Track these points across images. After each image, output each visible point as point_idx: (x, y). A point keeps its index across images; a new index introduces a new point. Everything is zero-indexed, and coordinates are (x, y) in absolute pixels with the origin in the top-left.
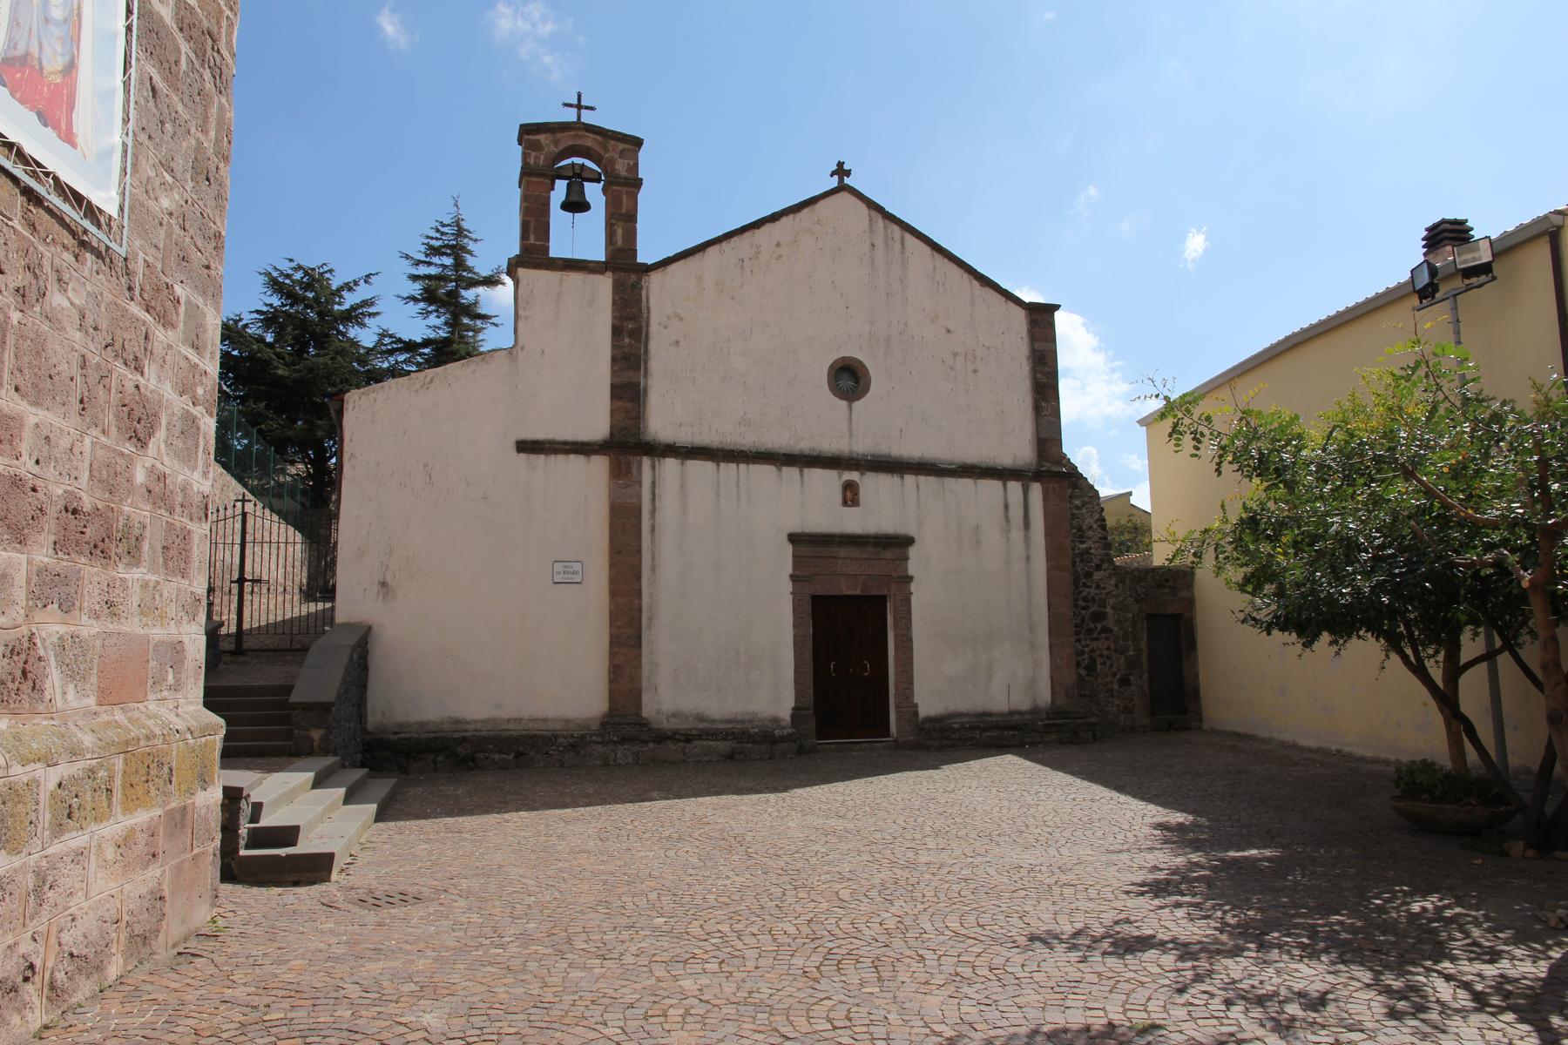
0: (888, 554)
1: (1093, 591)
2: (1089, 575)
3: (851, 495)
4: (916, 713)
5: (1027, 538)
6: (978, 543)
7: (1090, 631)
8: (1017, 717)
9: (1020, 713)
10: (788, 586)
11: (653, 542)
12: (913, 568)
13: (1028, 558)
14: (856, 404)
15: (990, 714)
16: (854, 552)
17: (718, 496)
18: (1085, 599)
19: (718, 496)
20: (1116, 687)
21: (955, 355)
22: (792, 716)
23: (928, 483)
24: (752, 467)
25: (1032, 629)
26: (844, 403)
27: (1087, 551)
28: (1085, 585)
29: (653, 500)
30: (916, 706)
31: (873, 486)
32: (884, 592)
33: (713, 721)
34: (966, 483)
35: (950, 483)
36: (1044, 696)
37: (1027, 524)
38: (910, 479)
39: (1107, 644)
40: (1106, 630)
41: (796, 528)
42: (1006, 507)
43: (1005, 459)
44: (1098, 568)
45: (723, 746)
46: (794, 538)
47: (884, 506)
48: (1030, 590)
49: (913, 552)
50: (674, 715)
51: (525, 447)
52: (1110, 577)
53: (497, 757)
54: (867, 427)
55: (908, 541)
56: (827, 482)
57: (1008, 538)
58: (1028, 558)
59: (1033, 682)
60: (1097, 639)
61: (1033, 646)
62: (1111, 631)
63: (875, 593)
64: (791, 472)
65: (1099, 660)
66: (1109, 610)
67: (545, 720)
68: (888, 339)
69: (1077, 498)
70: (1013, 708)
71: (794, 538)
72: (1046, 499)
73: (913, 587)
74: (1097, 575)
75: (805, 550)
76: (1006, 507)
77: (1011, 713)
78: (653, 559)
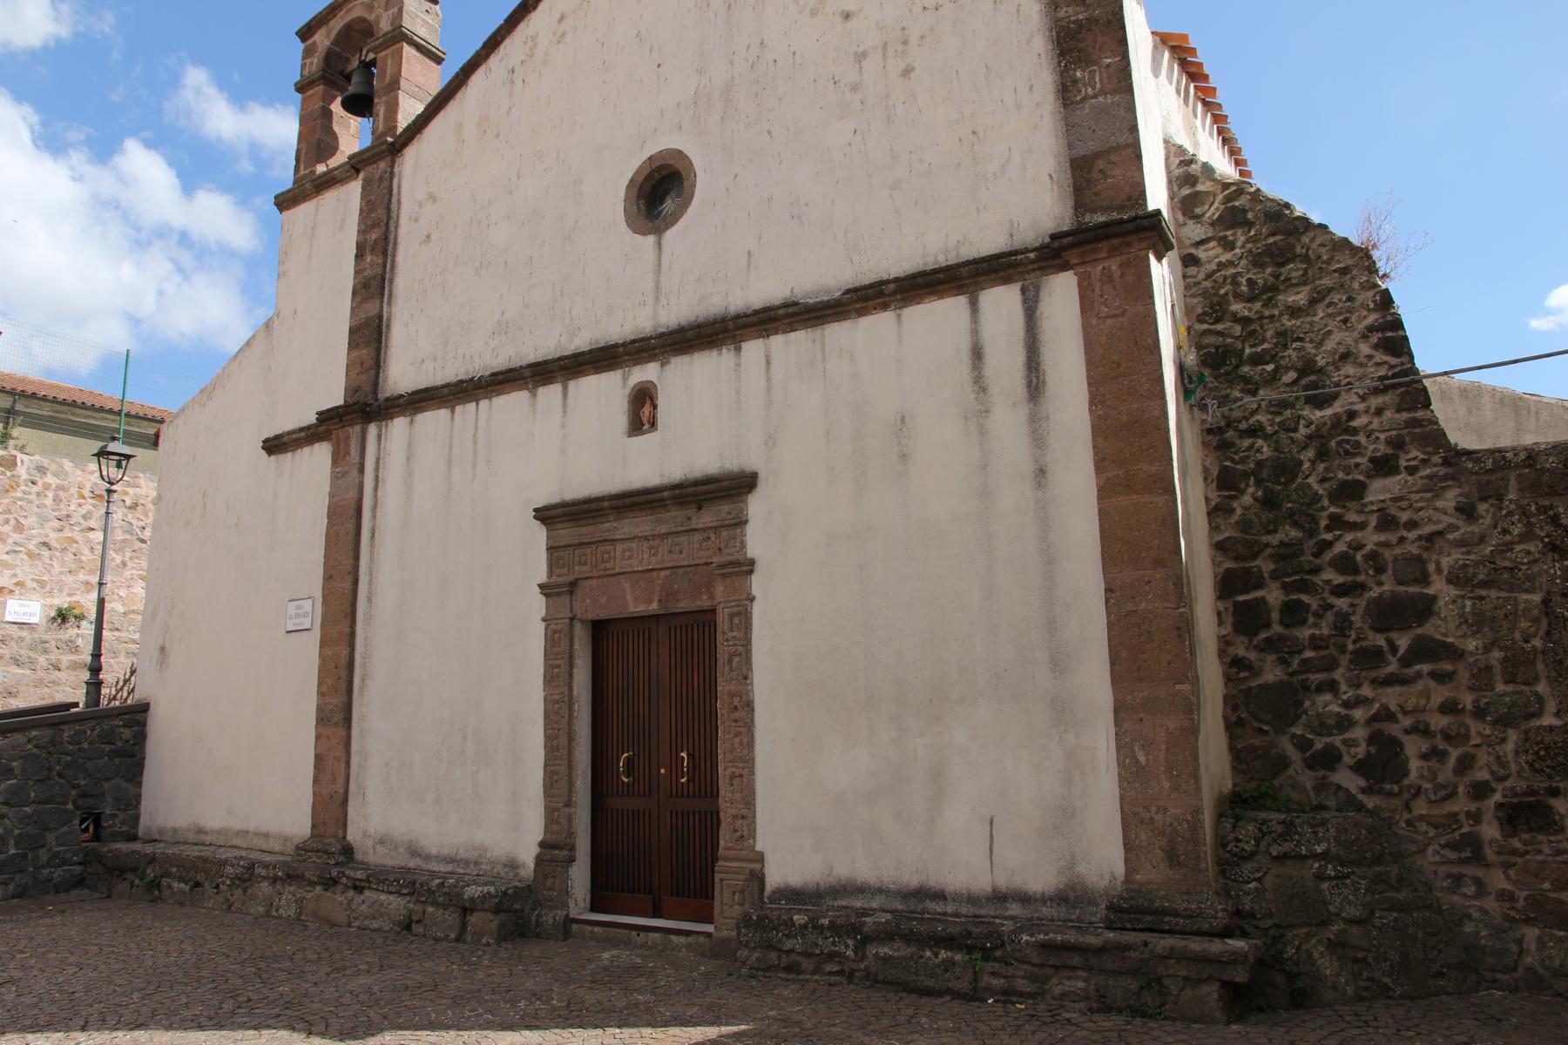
0: (707, 518)
1: (1371, 538)
2: (1351, 491)
3: (642, 411)
4: (759, 878)
5: (1037, 424)
6: (903, 457)
7: (1371, 657)
8: (1015, 909)
9: (1025, 898)
10: (538, 605)
11: (372, 553)
12: (757, 541)
13: (1041, 472)
14: (671, 234)
15: (940, 896)
16: (638, 525)
17: (449, 463)
18: (1345, 564)
19: (449, 463)
20: (1490, 830)
21: (861, 57)
22: (539, 860)
23: (801, 339)
24: (496, 400)
25: (1058, 664)
26: (651, 239)
27: (1342, 424)
28: (1337, 523)
29: (376, 488)
30: (760, 858)
31: (686, 383)
32: (704, 602)
33: (428, 858)
34: (879, 324)
35: (838, 333)
36: (1103, 856)
37: (1035, 384)
38: (753, 349)
39: (1440, 694)
40: (1425, 650)
41: (548, 494)
42: (977, 354)
43: (986, 238)
44: (1384, 466)
45: (396, 904)
46: (545, 515)
47: (706, 417)
48: (1049, 559)
49: (756, 506)
50: (381, 842)
51: (274, 446)
52: (1434, 487)
53: (176, 885)
54: (703, 265)
55: (740, 485)
56: (604, 393)
57: (982, 433)
58: (1041, 472)
59: (1064, 816)
60: (1391, 681)
61: (1061, 711)
62: (1456, 654)
63: (684, 605)
64: (550, 394)
65: (1413, 747)
66: (1439, 587)
67: (267, 836)
68: (729, 86)
69: (1290, 285)
70: (1003, 882)
71: (545, 515)
72: (1086, 306)
73: (757, 583)
74: (1380, 490)
75: (566, 534)
76: (977, 354)
77: (999, 897)
78: (370, 582)
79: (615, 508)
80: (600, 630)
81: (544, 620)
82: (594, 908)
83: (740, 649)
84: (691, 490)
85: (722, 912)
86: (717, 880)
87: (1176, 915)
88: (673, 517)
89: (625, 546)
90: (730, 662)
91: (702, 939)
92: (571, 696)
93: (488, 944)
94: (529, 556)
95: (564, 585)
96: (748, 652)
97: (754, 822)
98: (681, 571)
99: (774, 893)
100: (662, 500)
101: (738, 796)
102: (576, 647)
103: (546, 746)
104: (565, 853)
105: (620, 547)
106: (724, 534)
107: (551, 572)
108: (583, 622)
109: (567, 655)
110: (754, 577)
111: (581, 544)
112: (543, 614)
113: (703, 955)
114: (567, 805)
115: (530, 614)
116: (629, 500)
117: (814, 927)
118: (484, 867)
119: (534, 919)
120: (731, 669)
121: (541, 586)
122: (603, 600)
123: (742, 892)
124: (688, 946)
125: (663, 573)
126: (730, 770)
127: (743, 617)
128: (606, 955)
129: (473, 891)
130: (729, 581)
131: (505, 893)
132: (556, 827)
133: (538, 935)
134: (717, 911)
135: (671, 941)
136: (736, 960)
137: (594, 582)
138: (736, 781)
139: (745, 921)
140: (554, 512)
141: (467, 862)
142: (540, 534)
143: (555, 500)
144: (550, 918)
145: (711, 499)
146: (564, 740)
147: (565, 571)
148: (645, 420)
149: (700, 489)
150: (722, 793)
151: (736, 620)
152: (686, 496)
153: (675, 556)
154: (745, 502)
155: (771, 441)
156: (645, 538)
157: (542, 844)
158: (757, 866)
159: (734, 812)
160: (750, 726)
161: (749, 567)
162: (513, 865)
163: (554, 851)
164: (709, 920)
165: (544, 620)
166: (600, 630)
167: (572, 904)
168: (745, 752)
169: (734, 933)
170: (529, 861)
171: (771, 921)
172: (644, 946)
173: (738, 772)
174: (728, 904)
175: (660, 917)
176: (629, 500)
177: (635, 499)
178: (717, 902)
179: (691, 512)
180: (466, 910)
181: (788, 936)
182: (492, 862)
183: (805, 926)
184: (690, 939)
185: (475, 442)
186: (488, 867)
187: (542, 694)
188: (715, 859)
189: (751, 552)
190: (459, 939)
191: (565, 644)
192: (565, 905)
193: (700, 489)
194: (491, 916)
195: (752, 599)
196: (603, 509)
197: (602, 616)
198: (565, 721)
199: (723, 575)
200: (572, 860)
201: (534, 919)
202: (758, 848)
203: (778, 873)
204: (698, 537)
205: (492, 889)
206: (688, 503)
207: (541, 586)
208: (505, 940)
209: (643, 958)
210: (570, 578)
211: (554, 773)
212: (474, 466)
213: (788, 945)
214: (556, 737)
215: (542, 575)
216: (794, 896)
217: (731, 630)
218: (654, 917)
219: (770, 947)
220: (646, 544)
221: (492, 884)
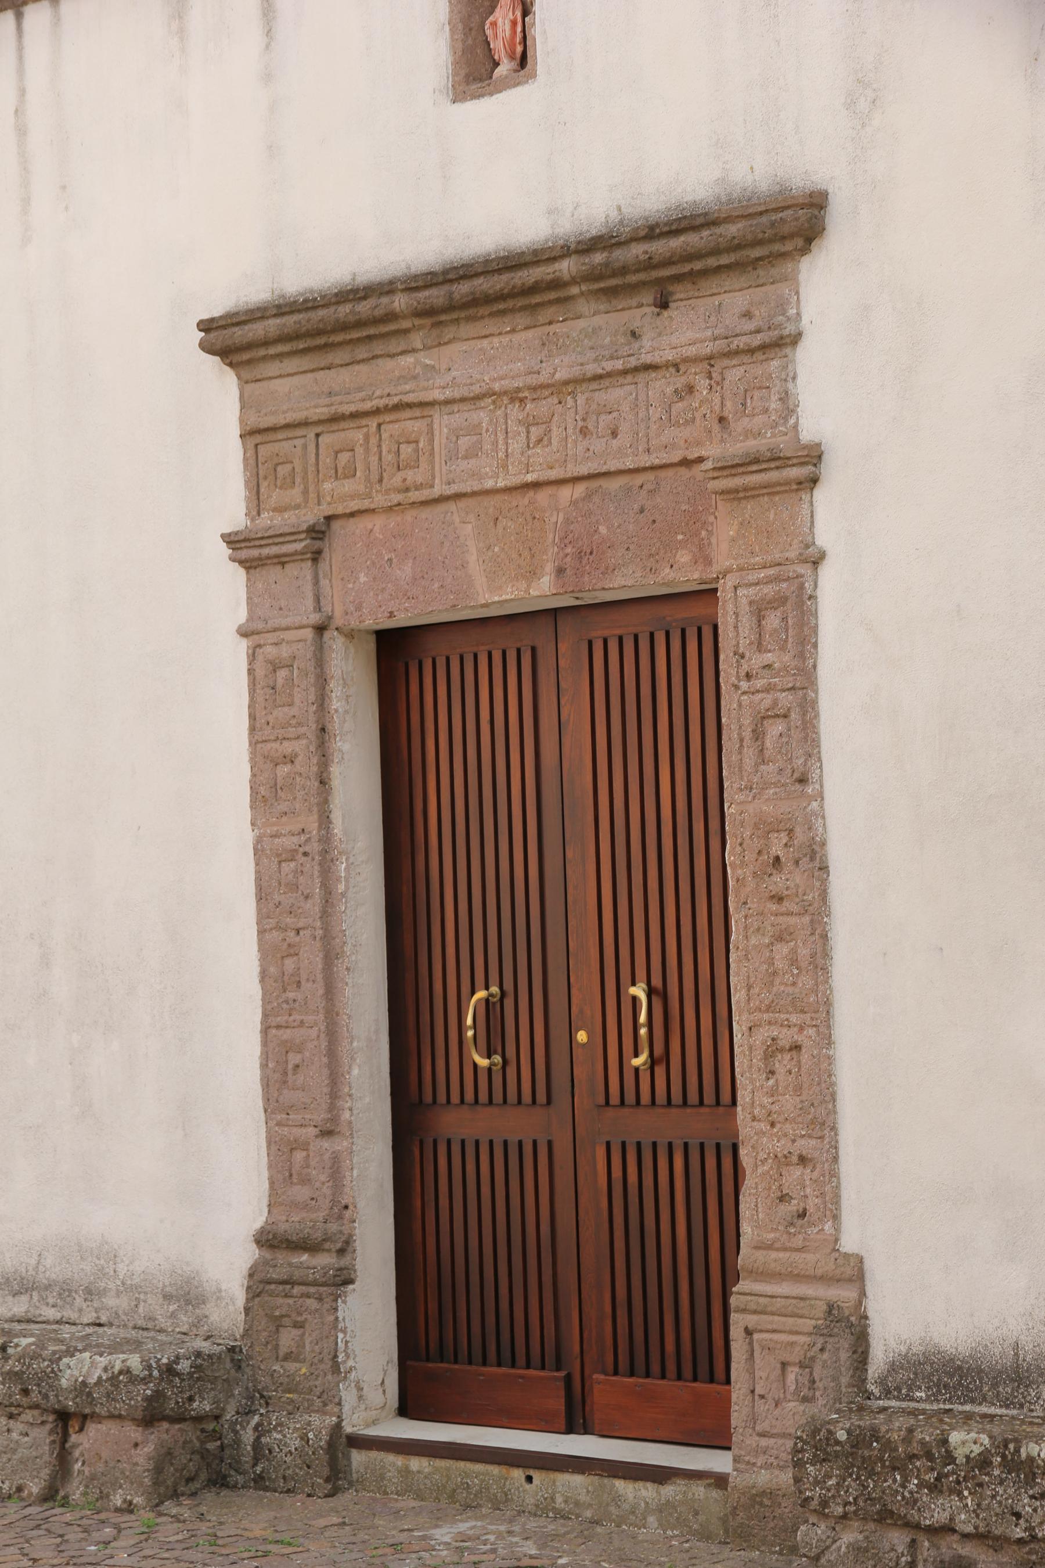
0: (686, 329)
4: (852, 1329)
12: (828, 393)
22: (260, 1284)
30: (854, 1272)
32: (681, 573)
41: (239, 277)
46: (233, 340)
49: (824, 289)
55: (784, 228)
63: (626, 581)
71: (233, 340)
75: (297, 389)
79: (427, 312)
80: (396, 652)
81: (244, 633)
82: (408, 1407)
83: (786, 699)
84: (637, 251)
85: (753, 1419)
86: (736, 1332)
87: (734, 366)
88: (593, 331)
89: (459, 418)
90: (758, 735)
91: (699, 1490)
92: (326, 838)
93: (129, 1508)
94: (192, 452)
95: (292, 534)
96: (808, 708)
97: (834, 1175)
98: (613, 485)
99: (893, 1367)
100: (556, 284)
101: (789, 1102)
102: (336, 704)
103: (264, 976)
104: (325, 1260)
105: (443, 423)
106: (734, 374)
107: (256, 501)
108: (350, 635)
109: (310, 730)
110: (820, 494)
111: (335, 419)
112: (242, 615)
113: (705, 1536)
114: (327, 1133)
115: (208, 613)
116: (463, 289)
117: (1005, 1463)
118: (111, 1301)
119: (248, 1436)
120: (762, 758)
121: (233, 541)
122: (405, 572)
123: (805, 1365)
124: (664, 1509)
125: (566, 493)
126: (763, 1034)
127: (792, 608)
128: (444, 1534)
129: (83, 1368)
130: (749, 507)
131: (170, 1371)
132: (300, 1193)
133: (260, 1482)
134: (737, 1419)
135: (617, 1499)
136: (794, 1550)
137: (377, 523)
138: (782, 1063)
139: (815, 1446)
140: (257, 330)
141: (65, 1291)
142: (220, 389)
143: (256, 293)
144: (293, 1435)
145: (693, 277)
146: (311, 957)
147: (295, 494)
148: (499, 47)
149: (659, 248)
150: (744, 1096)
151: (772, 620)
152: (624, 270)
153: (598, 445)
154: (791, 279)
155: (864, 94)
156: (515, 397)
157: (269, 1240)
158: (844, 1294)
159: (781, 1146)
160: (817, 912)
161: (804, 469)
162: (188, 1295)
163: (295, 1256)
164: (719, 1439)
165: (244, 633)
166: (396, 652)
167: (348, 1396)
168: (806, 981)
169: (785, 1478)
170: (236, 1290)
171: (888, 1445)
172: (544, 1509)
173: (786, 1037)
174: (769, 1392)
175: (586, 1431)
176: (463, 289)
177: (482, 285)
178: (738, 1391)
179: (639, 313)
180: (65, 1420)
181: (935, 1488)
182: (133, 1289)
183: (983, 1462)
184: (670, 1491)
185: (22, 132)
186: (123, 1303)
187: (248, 836)
188: (729, 1276)
189: (815, 421)
190: (50, 1495)
191: (303, 696)
192: (329, 1399)
193: (659, 248)
194: (134, 1432)
195: (817, 561)
196: (391, 317)
197: (402, 620)
198: (313, 907)
199: (733, 495)
200: (344, 1279)
201: (248, 1436)
202: (849, 1243)
203: (904, 1318)
204: (661, 386)
205: (135, 1362)
206: (634, 288)
207: (233, 541)
208: (175, 1495)
209: (545, 1541)
210: (311, 516)
211: (288, 1047)
212: (26, 202)
213: (938, 1511)
214: (291, 950)
215: (232, 510)
216: (954, 1378)
217: (760, 647)
218: (570, 1429)
219: (886, 1517)
220: (515, 412)
221: (136, 1345)
